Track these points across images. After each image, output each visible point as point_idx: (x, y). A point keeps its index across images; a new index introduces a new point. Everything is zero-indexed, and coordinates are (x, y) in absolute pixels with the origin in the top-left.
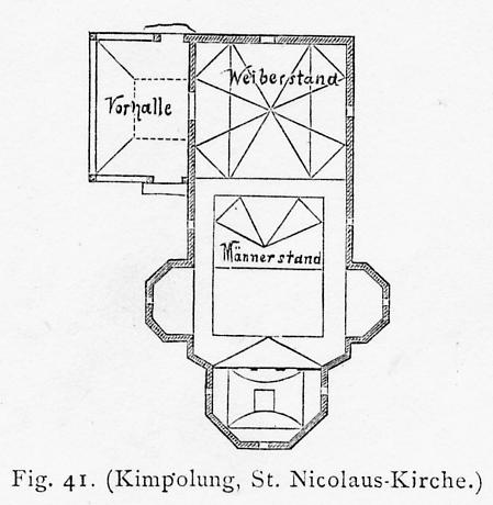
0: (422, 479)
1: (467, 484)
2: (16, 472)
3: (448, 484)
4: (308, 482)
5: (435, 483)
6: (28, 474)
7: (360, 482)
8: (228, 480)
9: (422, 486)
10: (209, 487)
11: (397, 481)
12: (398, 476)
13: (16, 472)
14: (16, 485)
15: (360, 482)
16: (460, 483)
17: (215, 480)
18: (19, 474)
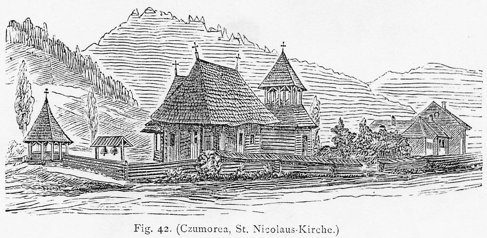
0: (215, 228)
1: (332, 231)
2: (136, 225)
3: (324, 231)
4: (261, 230)
5: (318, 231)
6: (142, 226)
7: (285, 230)
8: (147, 229)
9: (215, 232)
10: (324, 233)
11: (301, 229)
12: (302, 227)
13: (136, 225)
14: (136, 231)
15: (285, 230)
16: (329, 231)
17: (195, 230)
18: (137, 226)
